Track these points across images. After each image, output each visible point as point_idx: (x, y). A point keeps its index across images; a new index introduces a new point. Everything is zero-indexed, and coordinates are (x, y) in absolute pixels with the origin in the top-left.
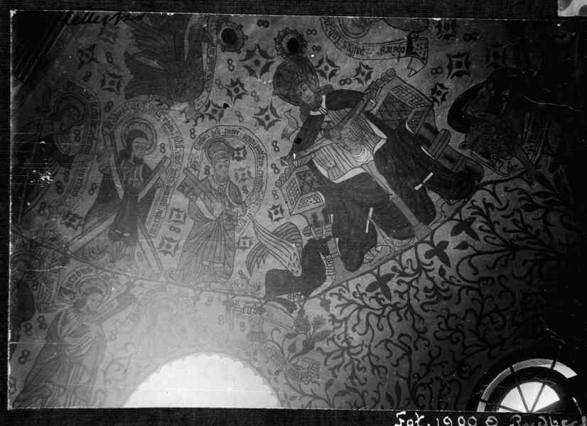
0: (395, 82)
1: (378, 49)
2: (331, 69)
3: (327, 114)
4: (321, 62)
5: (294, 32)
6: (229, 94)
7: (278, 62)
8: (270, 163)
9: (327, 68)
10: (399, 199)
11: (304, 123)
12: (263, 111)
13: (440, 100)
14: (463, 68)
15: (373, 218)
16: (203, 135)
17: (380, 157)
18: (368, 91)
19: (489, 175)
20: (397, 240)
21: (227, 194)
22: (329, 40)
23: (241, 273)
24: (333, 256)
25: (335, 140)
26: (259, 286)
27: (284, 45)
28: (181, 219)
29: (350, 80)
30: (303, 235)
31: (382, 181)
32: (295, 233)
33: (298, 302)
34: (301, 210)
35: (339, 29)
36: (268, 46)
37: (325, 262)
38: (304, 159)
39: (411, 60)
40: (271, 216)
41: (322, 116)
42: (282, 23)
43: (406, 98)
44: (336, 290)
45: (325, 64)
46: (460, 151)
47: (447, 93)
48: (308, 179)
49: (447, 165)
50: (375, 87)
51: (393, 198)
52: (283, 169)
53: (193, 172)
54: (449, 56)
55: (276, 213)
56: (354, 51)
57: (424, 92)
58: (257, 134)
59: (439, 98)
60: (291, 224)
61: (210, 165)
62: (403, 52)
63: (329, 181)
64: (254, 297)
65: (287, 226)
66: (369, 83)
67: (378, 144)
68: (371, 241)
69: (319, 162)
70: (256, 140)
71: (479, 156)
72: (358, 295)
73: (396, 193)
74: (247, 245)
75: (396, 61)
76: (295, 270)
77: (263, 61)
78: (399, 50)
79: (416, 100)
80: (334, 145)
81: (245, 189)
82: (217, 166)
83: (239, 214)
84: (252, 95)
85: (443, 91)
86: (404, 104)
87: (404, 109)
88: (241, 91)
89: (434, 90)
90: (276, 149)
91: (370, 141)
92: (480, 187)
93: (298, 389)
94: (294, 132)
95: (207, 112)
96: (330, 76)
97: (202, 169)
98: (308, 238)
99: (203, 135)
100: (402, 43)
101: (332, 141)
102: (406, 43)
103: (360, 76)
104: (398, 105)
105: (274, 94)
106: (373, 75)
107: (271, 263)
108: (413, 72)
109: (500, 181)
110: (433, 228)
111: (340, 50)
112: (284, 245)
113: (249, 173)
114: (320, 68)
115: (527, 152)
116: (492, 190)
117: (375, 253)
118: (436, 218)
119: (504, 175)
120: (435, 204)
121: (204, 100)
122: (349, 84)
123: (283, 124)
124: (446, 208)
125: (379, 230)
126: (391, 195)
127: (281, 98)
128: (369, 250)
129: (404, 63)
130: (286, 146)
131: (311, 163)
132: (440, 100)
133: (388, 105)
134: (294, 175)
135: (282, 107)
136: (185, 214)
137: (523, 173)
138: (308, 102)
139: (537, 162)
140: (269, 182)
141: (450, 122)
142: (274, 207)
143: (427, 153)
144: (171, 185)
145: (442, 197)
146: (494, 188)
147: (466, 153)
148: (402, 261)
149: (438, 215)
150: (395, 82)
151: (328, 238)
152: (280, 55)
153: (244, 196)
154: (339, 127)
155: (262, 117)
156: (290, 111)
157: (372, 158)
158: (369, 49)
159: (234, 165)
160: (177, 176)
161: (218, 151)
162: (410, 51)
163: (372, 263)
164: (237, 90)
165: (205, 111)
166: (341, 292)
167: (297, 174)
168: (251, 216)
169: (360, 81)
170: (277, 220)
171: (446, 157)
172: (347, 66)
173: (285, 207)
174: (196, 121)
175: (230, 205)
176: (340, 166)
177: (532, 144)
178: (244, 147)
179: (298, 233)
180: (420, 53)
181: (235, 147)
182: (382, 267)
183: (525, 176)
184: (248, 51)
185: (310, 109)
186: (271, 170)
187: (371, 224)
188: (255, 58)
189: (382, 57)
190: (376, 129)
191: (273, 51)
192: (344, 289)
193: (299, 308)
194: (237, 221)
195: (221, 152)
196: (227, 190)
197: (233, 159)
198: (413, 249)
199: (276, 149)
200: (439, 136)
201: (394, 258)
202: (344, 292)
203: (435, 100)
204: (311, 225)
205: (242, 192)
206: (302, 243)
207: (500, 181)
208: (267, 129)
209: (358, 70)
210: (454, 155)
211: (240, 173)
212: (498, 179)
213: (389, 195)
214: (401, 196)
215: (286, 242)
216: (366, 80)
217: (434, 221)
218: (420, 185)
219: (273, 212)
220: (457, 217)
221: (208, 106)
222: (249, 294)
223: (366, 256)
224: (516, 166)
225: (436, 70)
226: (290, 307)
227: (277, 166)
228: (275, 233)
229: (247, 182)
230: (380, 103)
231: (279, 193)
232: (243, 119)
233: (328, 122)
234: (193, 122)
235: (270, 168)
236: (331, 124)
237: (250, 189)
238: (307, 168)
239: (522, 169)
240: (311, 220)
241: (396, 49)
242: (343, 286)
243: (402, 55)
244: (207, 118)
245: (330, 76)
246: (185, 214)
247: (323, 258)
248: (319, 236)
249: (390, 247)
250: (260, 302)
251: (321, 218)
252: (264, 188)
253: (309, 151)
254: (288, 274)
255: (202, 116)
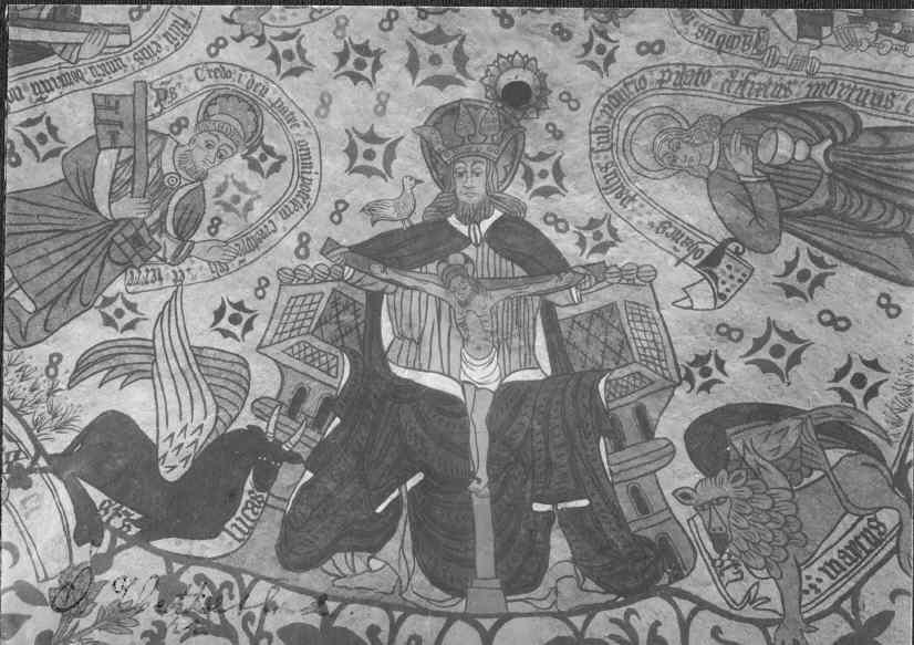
0: (643, 295)
1: (657, 218)
2: (550, 181)
3: (477, 245)
4: (542, 157)
5: (542, 77)
6: (343, 57)
7: (471, 91)
8: (303, 227)
9: (543, 174)
10: (487, 501)
11: (424, 224)
12: (371, 137)
13: (697, 385)
14: (781, 362)
15: (411, 494)
16: (232, 69)
17: (510, 398)
18: (582, 270)
19: (700, 581)
20: (423, 577)
21: (175, 201)
22: (587, 137)
23: (55, 360)
24: (271, 501)
25: (452, 300)
26: (66, 422)
27: (504, 80)
28: (42, 150)
29: (567, 228)
30: (247, 407)
31: (480, 442)
32: (237, 389)
33: (116, 533)
34: (285, 359)
35: (618, 135)
36: (478, 54)
37: (246, 497)
38: (369, 280)
39: (701, 280)
40: (219, 314)
41: (467, 241)
42: (534, 46)
43: (640, 336)
44: (217, 577)
45: (548, 165)
46: (672, 502)
47: (720, 382)
48: (347, 318)
49: (627, 508)
50: (599, 273)
51: (477, 492)
52: (315, 260)
53: (151, 103)
54: (771, 325)
55: (234, 320)
56: (614, 186)
57: (679, 350)
58: (326, 163)
59: (699, 381)
60: (246, 366)
61: (192, 123)
62: (695, 258)
63: (383, 356)
64: (33, 439)
65: (232, 362)
66: (594, 259)
67: (526, 372)
68: (370, 538)
69: (392, 308)
70: (316, 168)
71: (704, 534)
72: (253, 629)
73: (489, 485)
74: (121, 322)
75: (672, 261)
76: (172, 459)
77: (448, 68)
78: (694, 250)
79: (655, 354)
80: (445, 306)
81: (216, 223)
82: (202, 139)
83: (160, 254)
84: (378, 98)
85: (716, 374)
86: (628, 343)
87: (621, 350)
88: (367, 72)
89: (700, 361)
90: (337, 214)
91: (515, 356)
92: (669, 595)
93: (884, 133)
94: (393, 220)
95: (275, 43)
96: (539, 192)
97: (172, 115)
98: (253, 421)
99: (232, 69)
100: (706, 242)
101: (447, 294)
102: (712, 248)
103: (588, 235)
104: (614, 337)
105: (417, 131)
106: (612, 251)
107: (136, 402)
108: (686, 303)
109: (714, 609)
110: (513, 607)
111: (592, 168)
112: (195, 391)
113: (249, 207)
114: (532, 164)
115: (805, 587)
116: (686, 616)
117: (360, 566)
118: (532, 595)
119: (731, 602)
120: (550, 565)
121: (291, 21)
122: (559, 230)
123: (387, 190)
124: (568, 589)
125: (403, 528)
126: (479, 481)
127: (422, 147)
128: (354, 549)
129: (687, 274)
130: (357, 230)
131: (374, 300)
132: (697, 385)
133: (597, 322)
134: (327, 288)
135: (410, 161)
136: (59, 150)
137: (769, 623)
138: (463, 198)
139: (811, 619)
140: (270, 257)
141: (689, 436)
142: (239, 306)
143: (605, 460)
144: (88, 76)
145: (574, 561)
146: (694, 613)
147: (682, 512)
148: (401, 631)
149: (540, 591)
150: (643, 295)
151: (293, 458)
152: (486, 86)
153: (200, 235)
154: (478, 286)
155: (362, 146)
156: (418, 182)
157: (494, 387)
158: (642, 206)
159: (236, 165)
160: (115, 76)
161: (231, 117)
162: (709, 264)
163: (337, 583)
164: (360, 64)
165: (275, 39)
166: (225, 591)
167: (334, 290)
168: (179, 281)
169: (582, 243)
170: (226, 333)
171: (635, 493)
172: (581, 201)
173: (260, 326)
174: (243, 37)
175: (161, 222)
176: (425, 349)
177: (825, 577)
178: (283, 159)
179: (242, 393)
180: (723, 283)
181: (266, 141)
182: (351, 607)
183: (771, 631)
184: (439, 29)
185: (454, 211)
186: (292, 242)
187: (398, 500)
188: (439, 49)
189: (654, 237)
190: (540, 342)
191: (477, 69)
192: (236, 591)
193: (103, 549)
194: (145, 261)
195: (235, 123)
196: (181, 193)
197: (244, 157)
198: (442, 621)
199: (337, 214)
200: (650, 446)
201: (387, 608)
202: (232, 597)
203: (690, 378)
204: (282, 404)
205: (206, 223)
206: (233, 420)
207: (714, 609)
208: (351, 170)
209: (593, 224)
210: (654, 501)
211: (232, 190)
212: (714, 602)
213: (474, 478)
214: (495, 499)
215: (204, 386)
216: (593, 251)
217: (522, 596)
218: (547, 507)
219: (230, 311)
220: (578, 621)
221: (286, 37)
222: (28, 419)
223: (339, 557)
224: (768, 600)
225: (730, 330)
226: (87, 527)
227: (310, 245)
228: (198, 353)
229: (227, 217)
230: (586, 307)
231: (271, 293)
232: (325, 116)
233: (467, 259)
234: (236, 31)
235: (294, 235)
236: (470, 267)
237: (225, 233)
238: (361, 297)
239: (775, 611)
240: (287, 397)
241: (688, 243)
242: (240, 581)
243: (690, 260)
244: (266, 50)
245: (539, 192)
246: (59, 150)
247: (248, 486)
248: (279, 436)
249: (399, 580)
250: (35, 461)
251: (311, 405)
252: (249, 258)
253: (391, 275)
254: (146, 452)
255: (262, 40)
